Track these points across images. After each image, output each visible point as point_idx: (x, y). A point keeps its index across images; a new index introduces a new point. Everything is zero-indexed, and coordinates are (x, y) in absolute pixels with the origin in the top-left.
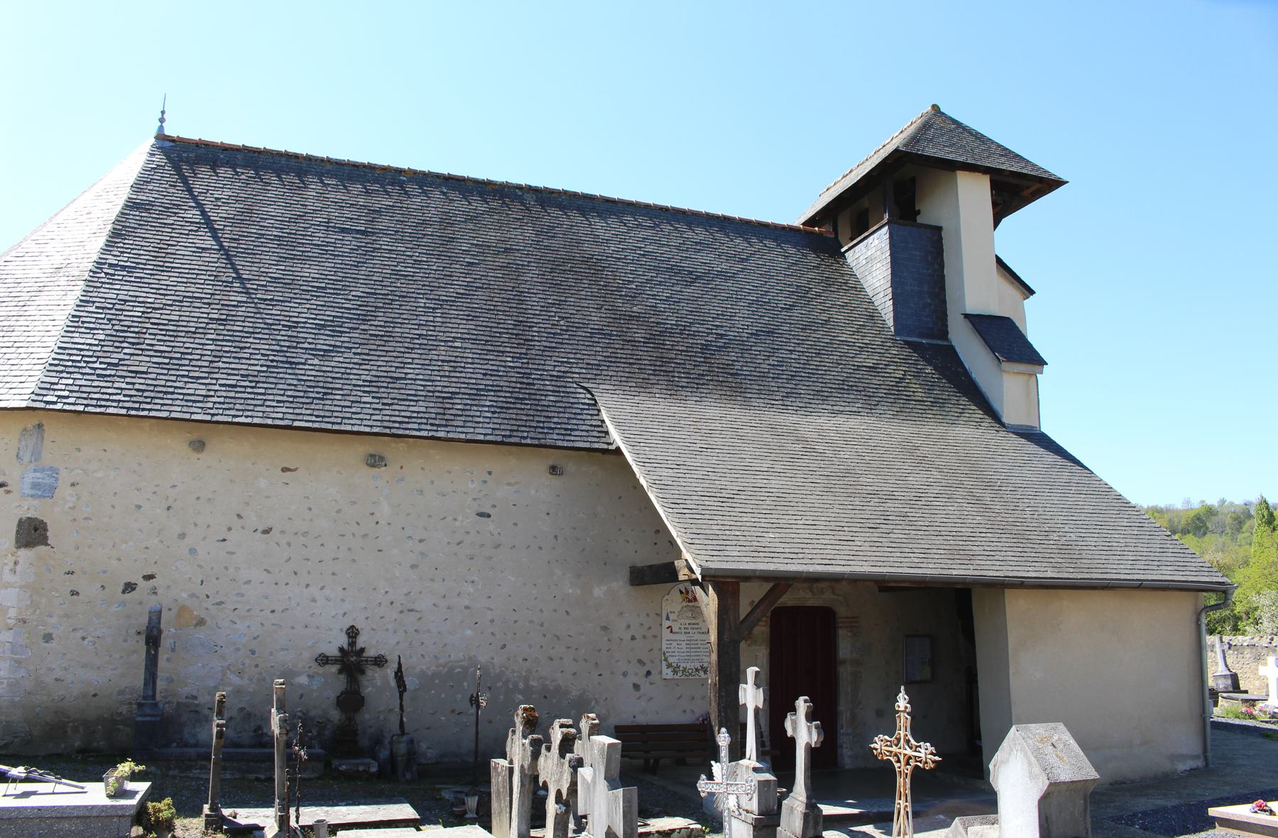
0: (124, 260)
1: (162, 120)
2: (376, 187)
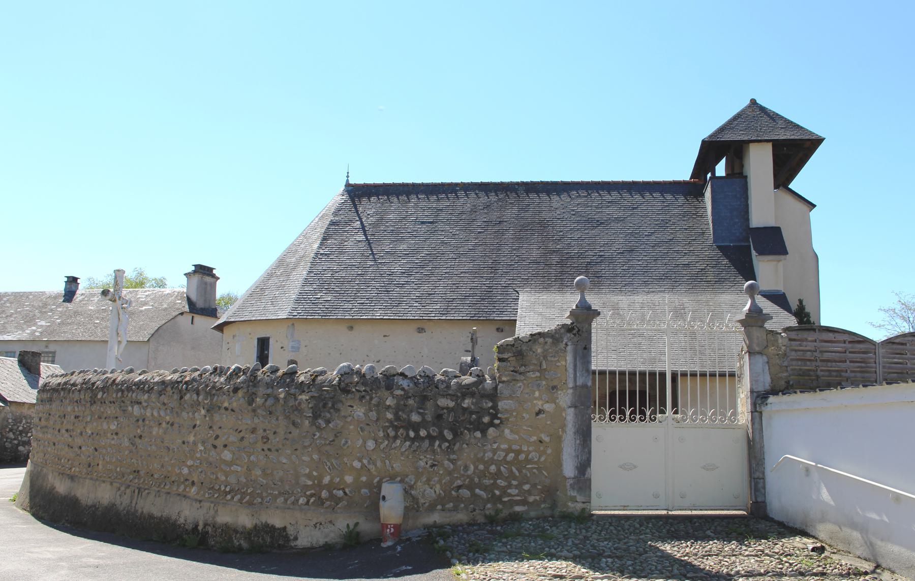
0: (326, 251)
1: (348, 177)
2: (443, 196)
